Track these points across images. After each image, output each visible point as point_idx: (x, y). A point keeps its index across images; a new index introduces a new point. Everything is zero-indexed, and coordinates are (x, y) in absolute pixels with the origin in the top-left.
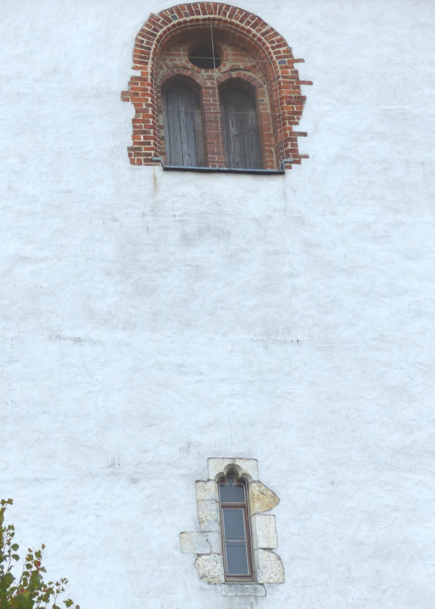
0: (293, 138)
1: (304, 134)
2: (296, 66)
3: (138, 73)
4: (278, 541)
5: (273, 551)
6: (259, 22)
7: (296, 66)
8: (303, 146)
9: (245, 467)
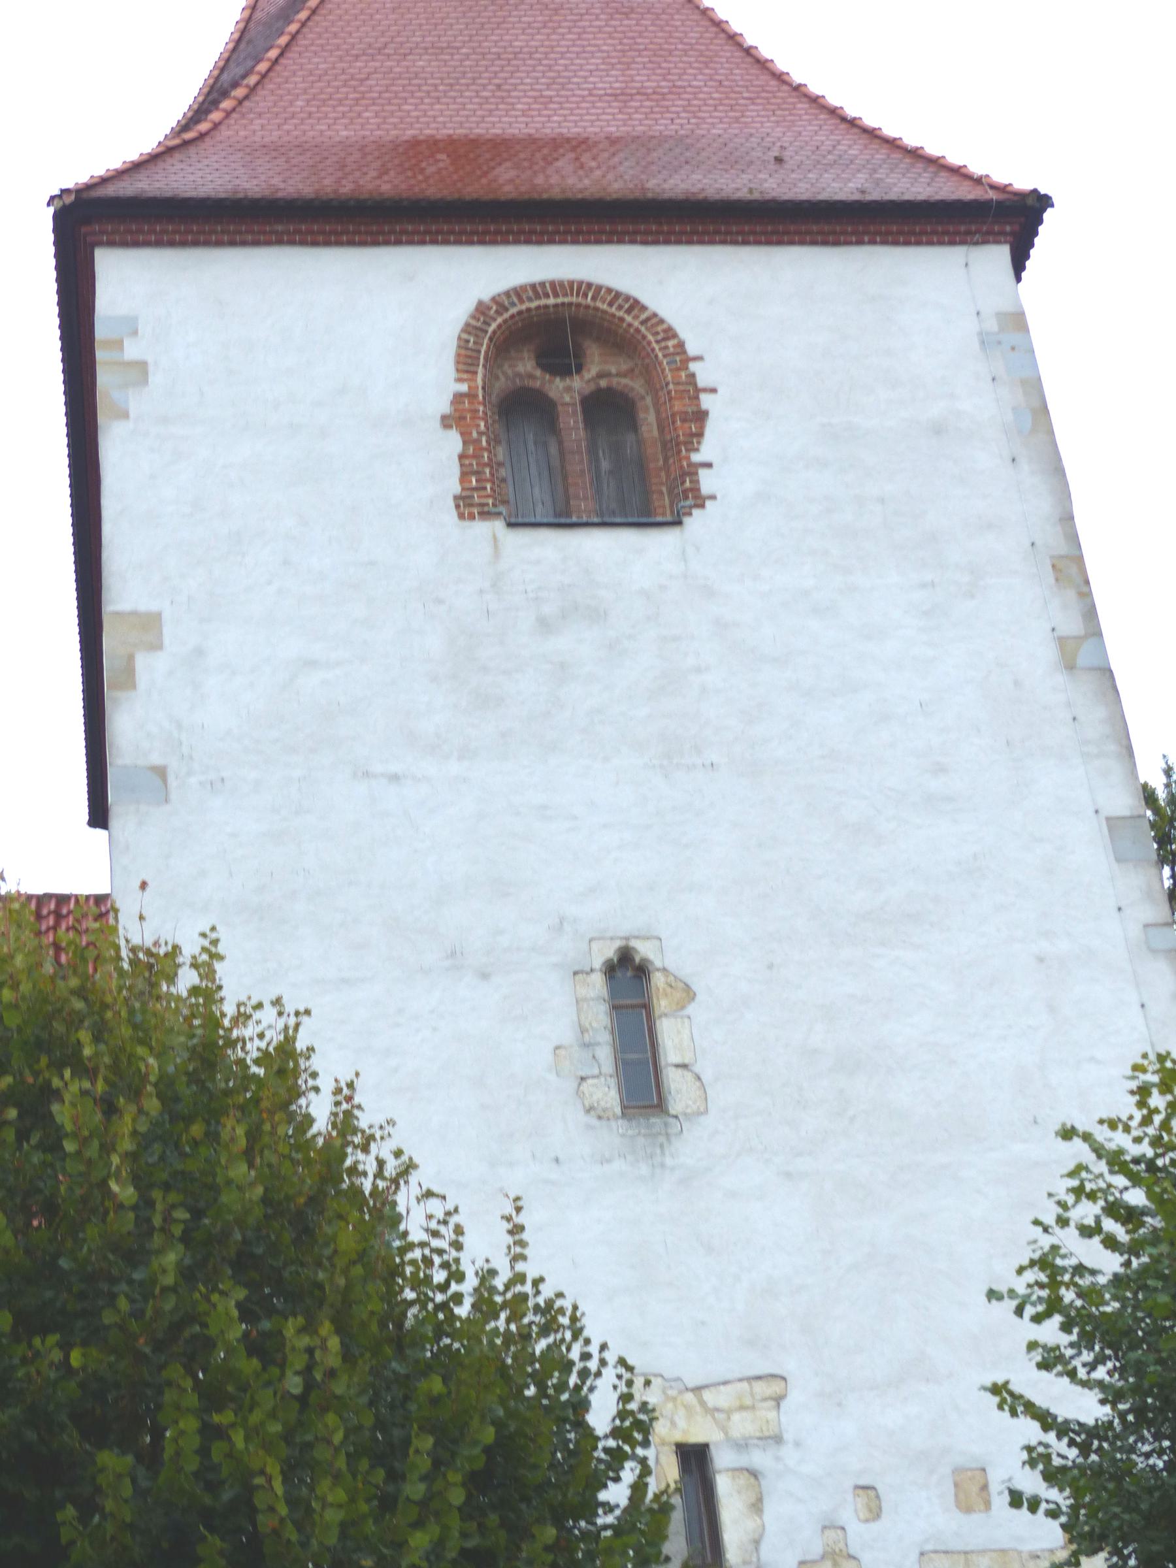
2: (693, 367)
3: (464, 388)
6: (635, 305)
7: (693, 367)
8: (707, 482)
9: (644, 950)
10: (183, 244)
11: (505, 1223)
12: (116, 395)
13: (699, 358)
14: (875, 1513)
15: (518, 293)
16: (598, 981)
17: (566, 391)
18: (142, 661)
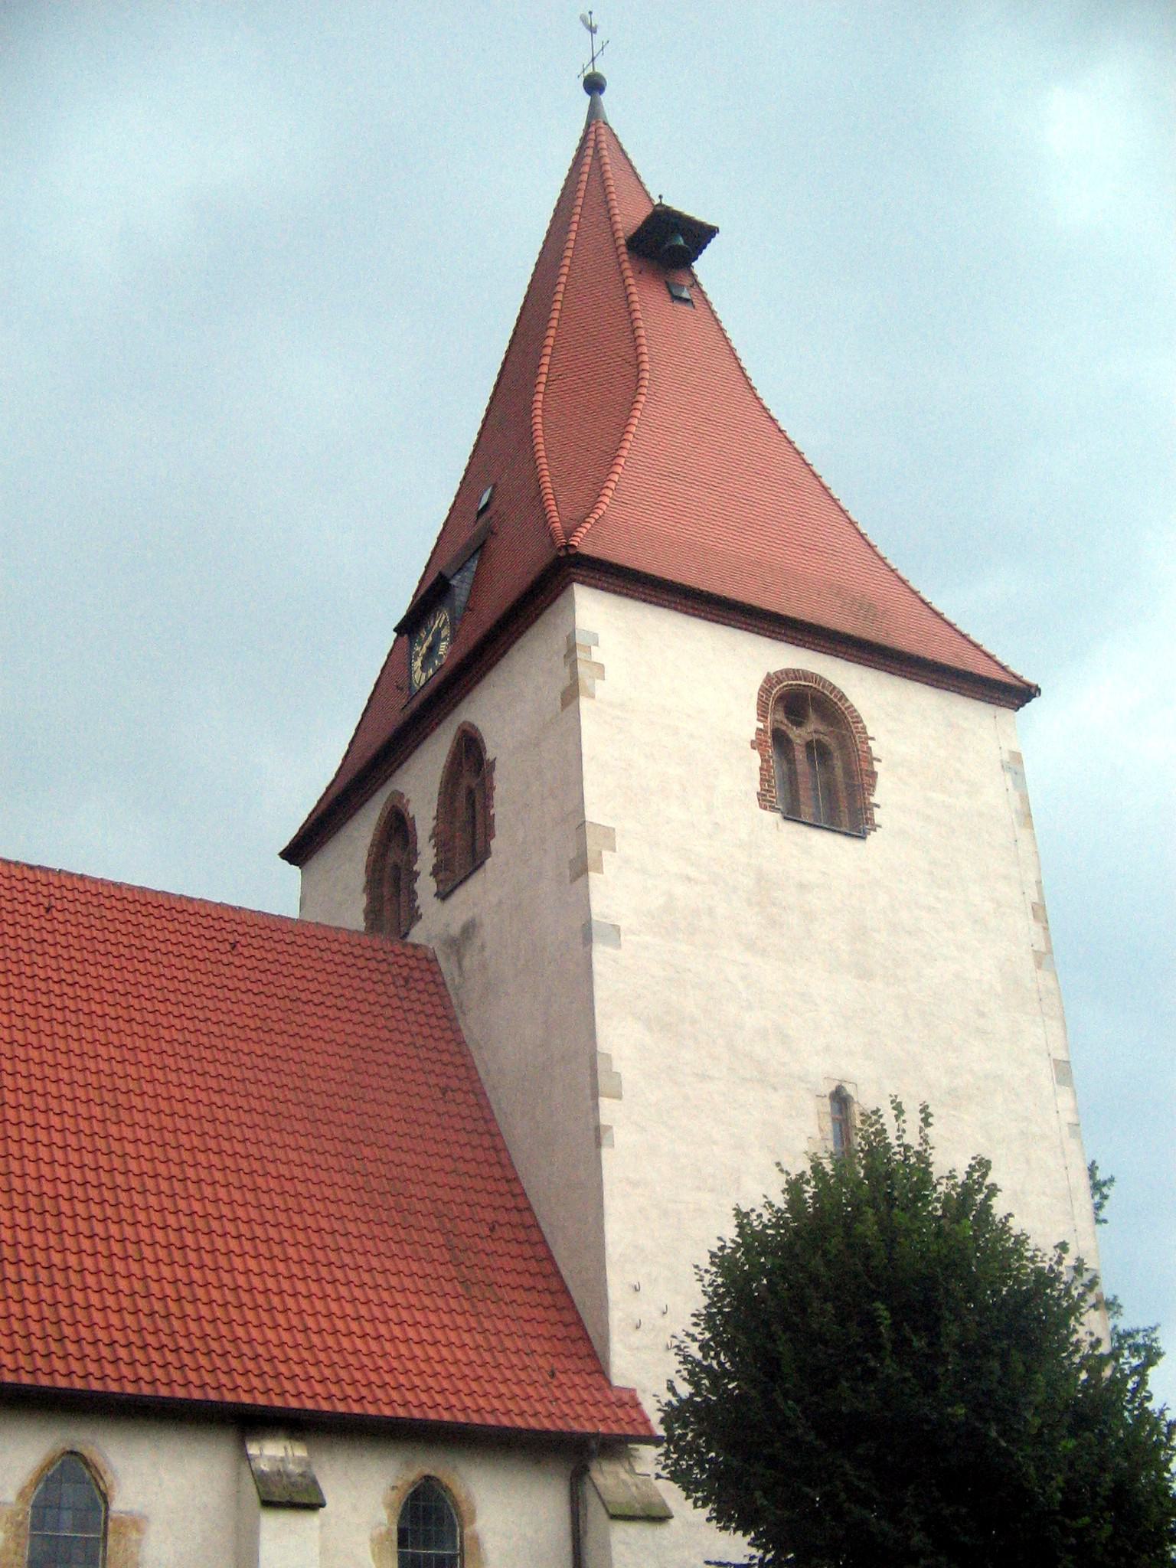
0: (869, 808)
1: (878, 806)
2: (871, 743)
3: (761, 726)
4: (306, 1501)
5: (1061, 1055)
6: (843, 697)
7: (871, 743)
8: (878, 816)
9: (849, 1089)
10: (620, 594)
11: (1108, 1295)
12: (588, 682)
13: (872, 739)
14: (670, 1382)
15: (786, 673)
16: (827, 1101)
17: (798, 736)
18: (606, 855)
